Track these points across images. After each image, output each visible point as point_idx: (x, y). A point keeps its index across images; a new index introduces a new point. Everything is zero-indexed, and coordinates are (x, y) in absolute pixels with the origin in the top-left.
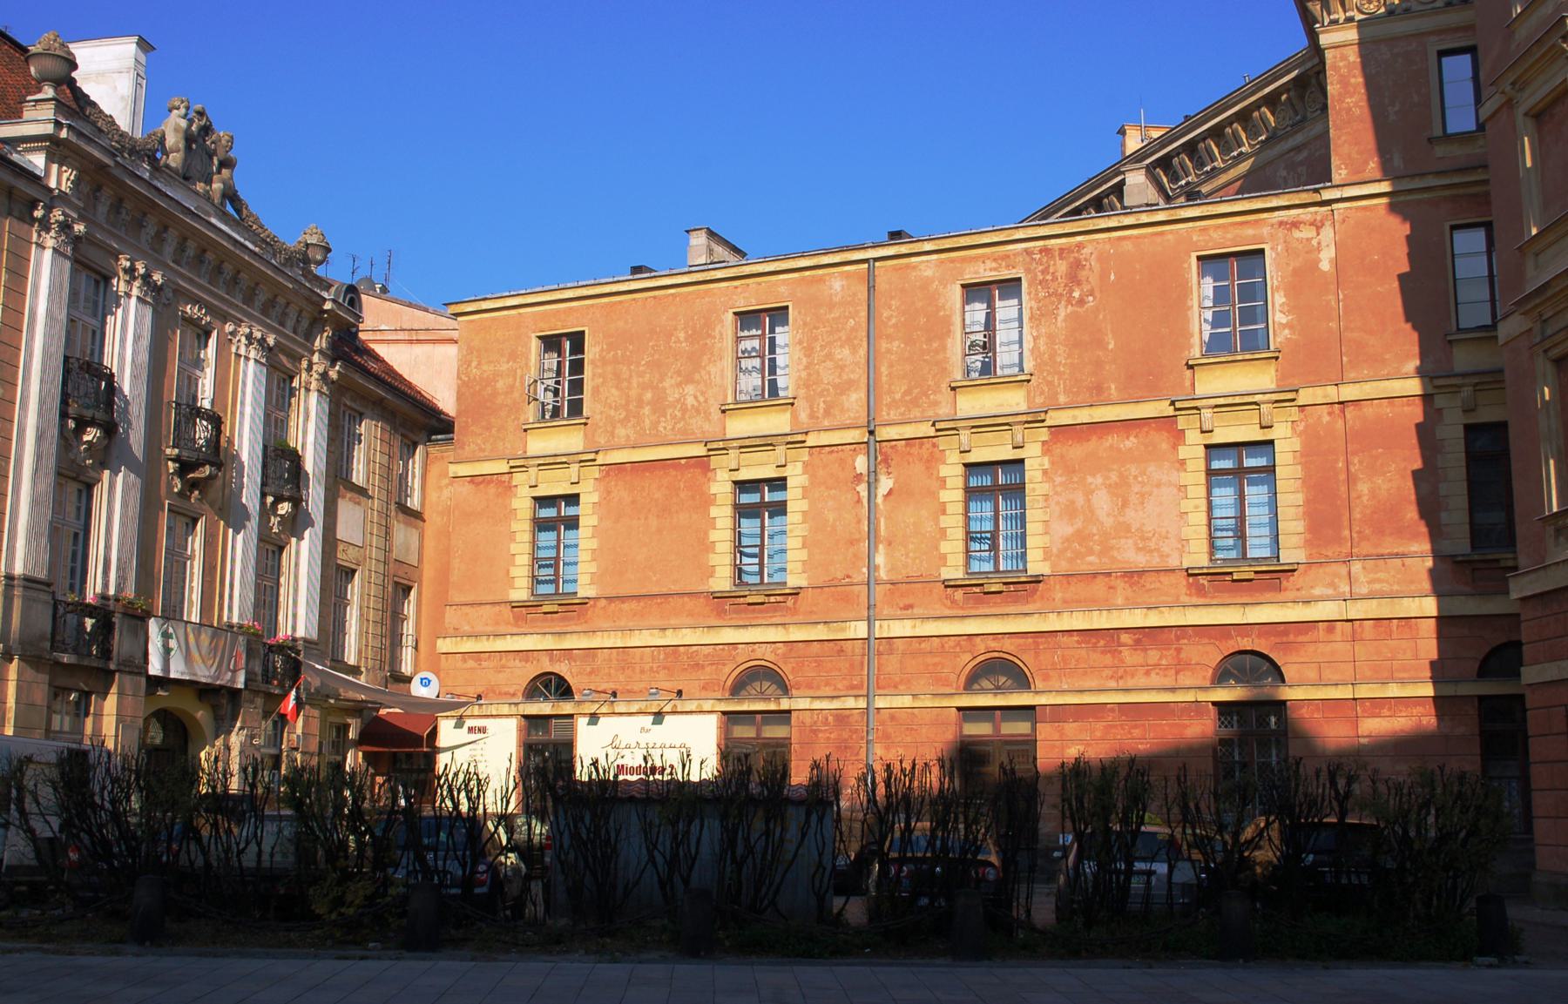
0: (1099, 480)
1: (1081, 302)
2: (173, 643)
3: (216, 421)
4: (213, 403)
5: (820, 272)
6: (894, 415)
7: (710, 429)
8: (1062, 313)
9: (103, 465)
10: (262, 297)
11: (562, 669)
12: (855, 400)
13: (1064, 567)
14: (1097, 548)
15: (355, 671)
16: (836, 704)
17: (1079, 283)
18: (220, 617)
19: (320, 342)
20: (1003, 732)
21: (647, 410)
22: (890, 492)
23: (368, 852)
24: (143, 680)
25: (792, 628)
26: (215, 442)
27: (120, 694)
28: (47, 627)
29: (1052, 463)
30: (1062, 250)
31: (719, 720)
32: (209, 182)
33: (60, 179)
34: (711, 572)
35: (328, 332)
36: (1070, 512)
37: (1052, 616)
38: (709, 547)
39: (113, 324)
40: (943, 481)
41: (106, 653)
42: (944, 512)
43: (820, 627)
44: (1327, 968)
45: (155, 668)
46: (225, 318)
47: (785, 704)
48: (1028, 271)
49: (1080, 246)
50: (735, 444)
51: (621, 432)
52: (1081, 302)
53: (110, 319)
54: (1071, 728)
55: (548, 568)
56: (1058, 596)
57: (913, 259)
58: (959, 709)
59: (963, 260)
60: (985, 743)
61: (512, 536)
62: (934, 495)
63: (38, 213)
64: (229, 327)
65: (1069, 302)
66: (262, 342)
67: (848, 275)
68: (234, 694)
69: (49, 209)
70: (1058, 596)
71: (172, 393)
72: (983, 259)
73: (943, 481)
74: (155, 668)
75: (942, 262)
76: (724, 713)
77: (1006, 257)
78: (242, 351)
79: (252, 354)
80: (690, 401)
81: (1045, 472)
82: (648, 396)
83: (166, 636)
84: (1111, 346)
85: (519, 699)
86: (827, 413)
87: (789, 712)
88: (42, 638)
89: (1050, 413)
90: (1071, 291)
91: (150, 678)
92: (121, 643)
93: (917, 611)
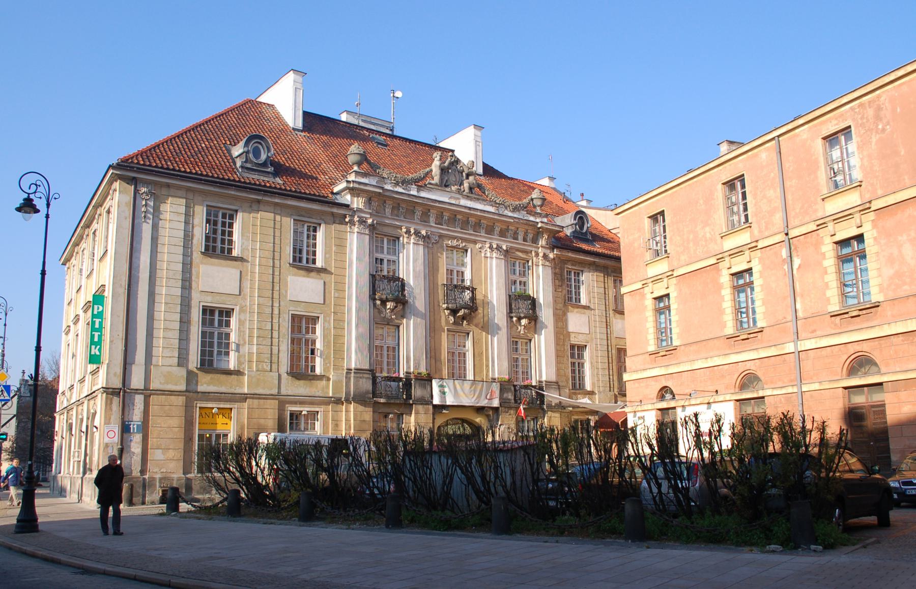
0: (905, 237)
1: (883, 130)
2: (446, 390)
3: (473, 290)
4: (472, 281)
5: (755, 151)
6: (797, 223)
7: (715, 248)
8: (874, 140)
9: (403, 317)
10: (497, 230)
11: (669, 384)
12: (779, 217)
13: (891, 295)
14: (908, 280)
15: (591, 393)
16: (784, 391)
17: (881, 120)
18: (487, 375)
19: (542, 242)
20: (853, 402)
21: (691, 244)
22: (800, 266)
23: (570, 484)
24: (431, 407)
25: (760, 351)
26: (473, 299)
27: (416, 413)
28: (370, 388)
29: (878, 232)
30: (870, 102)
31: (735, 405)
32: (461, 184)
33: (358, 203)
34: (724, 325)
35: (546, 236)
36: (891, 260)
37: (886, 326)
38: (722, 312)
39: (402, 257)
40: (824, 254)
41: (409, 396)
42: (826, 273)
43: (773, 348)
44: (648, 548)
45: (436, 401)
46: (475, 242)
47: (761, 394)
48: (854, 120)
49: (879, 97)
50: (727, 254)
51: (683, 258)
52: (883, 130)
53: (401, 255)
54: (903, 395)
55: (663, 333)
56: (889, 313)
57: (797, 131)
58: (845, 388)
59: (821, 123)
60: (862, 408)
61: (646, 320)
62: (820, 264)
63: (347, 220)
64: (479, 246)
65: (877, 132)
66: (499, 248)
67: (768, 149)
68: (496, 410)
69: (352, 216)
70: (889, 313)
71: (442, 278)
72: (830, 120)
73: (824, 254)
74: (436, 401)
75: (810, 128)
76: (737, 400)
77: (842, 115)
78: (488, 255)
79: (494, 255)
80: (708, 235)
81: (875, 239)
82: (691, 236)
83: (442, 386)
84: (902, 153)
85: (655, 401)
86: (767, 228)
87: (763, 397)
88: (367, 392)
89: (873, 202)
90: (878, 125)
91: (435, 406)
92: (417, 392)
93: (819, 333)
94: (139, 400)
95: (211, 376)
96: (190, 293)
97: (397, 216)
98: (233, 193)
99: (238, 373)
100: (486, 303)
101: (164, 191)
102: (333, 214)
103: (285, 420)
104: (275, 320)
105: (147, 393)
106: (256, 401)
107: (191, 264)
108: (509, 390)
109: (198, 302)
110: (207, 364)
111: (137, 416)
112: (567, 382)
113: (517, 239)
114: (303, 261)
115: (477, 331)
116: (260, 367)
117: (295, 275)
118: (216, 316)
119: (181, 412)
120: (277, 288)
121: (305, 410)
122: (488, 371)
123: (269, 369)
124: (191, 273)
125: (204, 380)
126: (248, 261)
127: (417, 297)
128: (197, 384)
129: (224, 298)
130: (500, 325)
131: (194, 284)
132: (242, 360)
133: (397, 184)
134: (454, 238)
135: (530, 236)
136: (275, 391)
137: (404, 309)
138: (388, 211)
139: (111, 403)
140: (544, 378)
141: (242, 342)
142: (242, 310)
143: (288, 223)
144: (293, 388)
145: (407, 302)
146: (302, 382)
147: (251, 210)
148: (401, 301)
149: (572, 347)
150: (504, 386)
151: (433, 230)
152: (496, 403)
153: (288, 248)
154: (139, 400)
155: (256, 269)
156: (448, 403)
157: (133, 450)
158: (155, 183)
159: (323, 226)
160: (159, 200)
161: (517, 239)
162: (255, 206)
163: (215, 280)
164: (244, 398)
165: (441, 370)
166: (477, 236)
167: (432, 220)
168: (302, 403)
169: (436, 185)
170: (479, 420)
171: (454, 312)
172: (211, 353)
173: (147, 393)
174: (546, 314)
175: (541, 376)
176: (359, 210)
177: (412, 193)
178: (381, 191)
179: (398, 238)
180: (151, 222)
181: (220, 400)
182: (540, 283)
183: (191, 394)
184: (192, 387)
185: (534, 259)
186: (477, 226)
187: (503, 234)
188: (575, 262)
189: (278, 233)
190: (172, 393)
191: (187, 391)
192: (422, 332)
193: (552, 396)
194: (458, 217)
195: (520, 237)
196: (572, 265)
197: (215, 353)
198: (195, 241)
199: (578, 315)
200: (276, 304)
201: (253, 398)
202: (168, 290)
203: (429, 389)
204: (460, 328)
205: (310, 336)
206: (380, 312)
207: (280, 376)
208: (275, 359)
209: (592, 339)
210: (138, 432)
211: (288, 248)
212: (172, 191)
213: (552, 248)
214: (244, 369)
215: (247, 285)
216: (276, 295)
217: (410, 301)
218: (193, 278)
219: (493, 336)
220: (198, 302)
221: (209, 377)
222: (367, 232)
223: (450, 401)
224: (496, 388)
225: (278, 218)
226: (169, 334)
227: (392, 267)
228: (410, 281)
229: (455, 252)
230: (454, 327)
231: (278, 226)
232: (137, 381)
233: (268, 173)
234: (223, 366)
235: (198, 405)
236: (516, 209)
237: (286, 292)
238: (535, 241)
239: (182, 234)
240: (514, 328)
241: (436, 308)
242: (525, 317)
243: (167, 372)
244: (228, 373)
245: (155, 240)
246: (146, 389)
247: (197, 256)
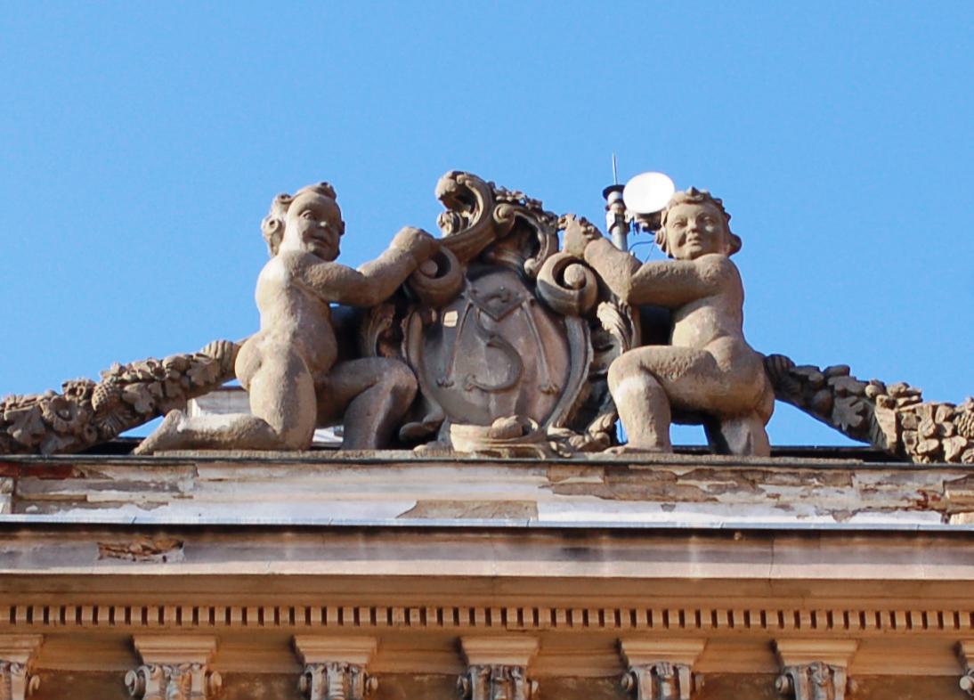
194: (486, 652)
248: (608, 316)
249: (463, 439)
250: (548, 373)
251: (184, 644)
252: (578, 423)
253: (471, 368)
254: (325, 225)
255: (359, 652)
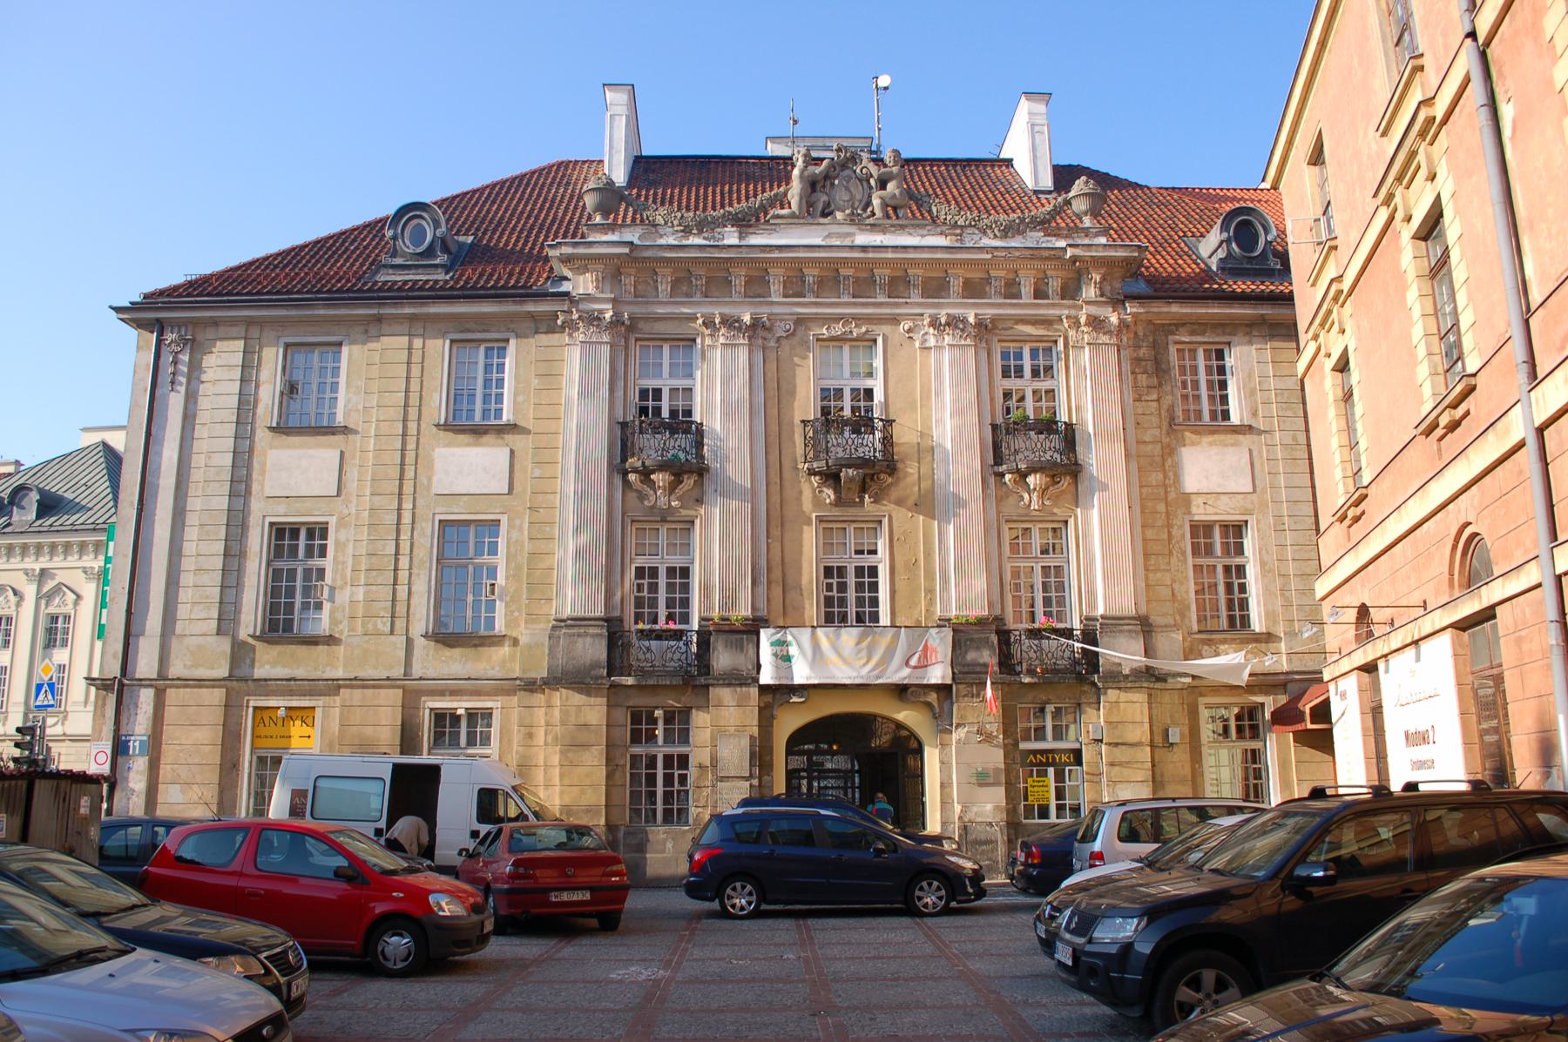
2: (793, 650)
19: (1090, 292)
24: (754, 691)
31: (1455, 644)
45: (766, 677)
46: (895, 320)
66: (731, 323)
68: (943, 690)
71: (806, 406)
74: (766, 677)
88: (595, 665)
92: (722, 659)
94: (146, 697)
95: (279, 648)
96: (246, 504)
97: (688, 295)
98: (322, 312)
99: (331, 640)
100: (926, 450)
101: (210, 333)
102: (532, 316)
103: (419, 727)
104: (405, 536)
105: (162, 684)
106: (358, 692)
107: (251, 450)
108: (980, 644)
109: (262, 514)
110: (280, 626)
111: (140, 726)
112: (1183, 612)
113: (1018, 296)
114: (471, 423)
115: (901, 515)
116: (370, 627)
117: (448, 445)
118: (296, 541)
119: (218, 716)
120: (410, 473)
121: (461, 706)
122: (931, 602)
123: (387, 629)
124: (249, 467)
125: (266, 657)
126: (356, 432)
127: (732, 456)
128: (252, 665)
129: (309, 504)
130: (964, 495)
131: (255, 488)
132: (339, 615)
133: (687, 231)
134: (837, 319)
135: (1054, 284)
136: (398, 672)
137: (700, 484)
138: (664, 288)
139: (104, 705)
140: (1101, 611)
141: (339, 583)
142: (342, 523)
143: (438, 349)
144: (434, 663)
145: (707, 469)
146: (457, 651)
147: (368, 337)
148: (693, 472)
149: (1201, 530)
150: (963, 635)
151: (776, 310)
152: (938, 674)
153: (436, 396)
154: (146, 697)
155: (372, 445)
156: (797, 681)
157: (131, 785)
158: (196, 323)
159: (513, 342)
160: (197, 347)
161: (1018, 296)
162: (373, 330)
163: (295, 475)
164: (333, 687)
165: (800, 609)
166: (897, 305)
167: (776, 289)
168: (454, 693)
169: (793, 216)
170: (906, 715)
171: (831, 477)
172: (290, 607)
173: (162, 684)
174: (1104, 459)
175: (1092, 604)
176: (588, 298)
177: (726, 242)
178: (626, 250)
179: (694, 340)
180: (182, 389)
181: (291, 693)
182: (1087, 388)
183: (239, 681)
184: (238, 673)
185: (1071, 333)
186: (898, 284)
187: (973, 290)
188: (1198, 326)
189: (416, 371)
190: (200, 683)
191: (231, 677)
192: (742, 530)
193: (1121, 653)
194: (843, 272)
195: (1027, 290)
196: (1193, 333)
197: (298, 605)
198: (260, 410)
199: (1215, 450)
200: (407, 505)
201: (351, 687)
202: (209, 501)
203: (752, 651)
204: (851, 512)
205: (486, 559)
206: (642, 497)
207: (409, 643)
208: (401, 609)
209: (1263, 505)
210: (141, 754)
211: (436, 396)
212: (222, 331)
213: (1117, 302)
214: (341, 632)
215: (352, 474)
216: (408, 487)
217: (714, 465)
218: (255, 476)
219: (944, 520)
220: (262, 514)
221: (276, 650)
222: (606, 338)
223: (802, 674)
224: (940, 643)
225: (418, 343)
226: (205, 579)
227: (1173, 397)
228: (1088, 422)
229: (846, 349)
230: (836, 512)
231: (417, 357)
232: (145, 665)
233: (436, 266)
234: (310, 629)
235: (252, 704)
236: (1006, 232)
237: (430, 479)
238: (1070, 291)
239: (234, 401)
240: (1012, 500)
241: (787, 475)
242: (1033, 470)
243: (201, 650)
244: (313, 641)
245: (189, 419)
246: (162, 676)
247: (262, 436)
248: (872, 182)
249: (839, 215)
250: (858, 197)
251: (246, 771)
252: (864, 210)
253: (841, 196)
254: (1418, 659)
255: (816, 272)
